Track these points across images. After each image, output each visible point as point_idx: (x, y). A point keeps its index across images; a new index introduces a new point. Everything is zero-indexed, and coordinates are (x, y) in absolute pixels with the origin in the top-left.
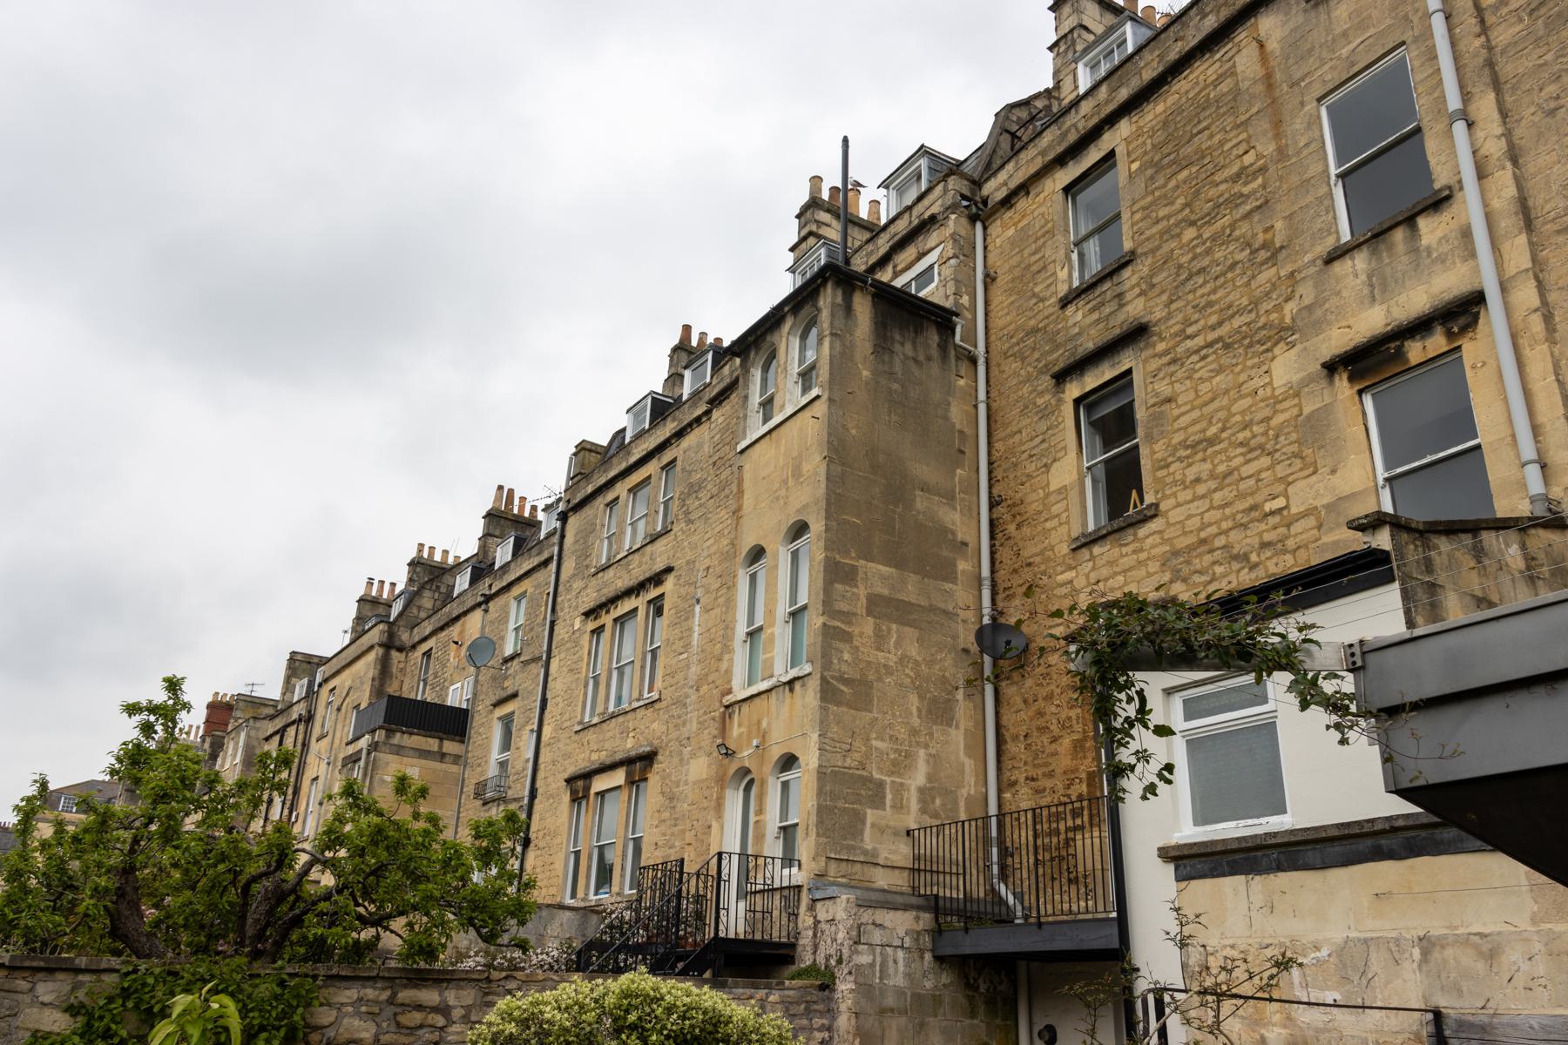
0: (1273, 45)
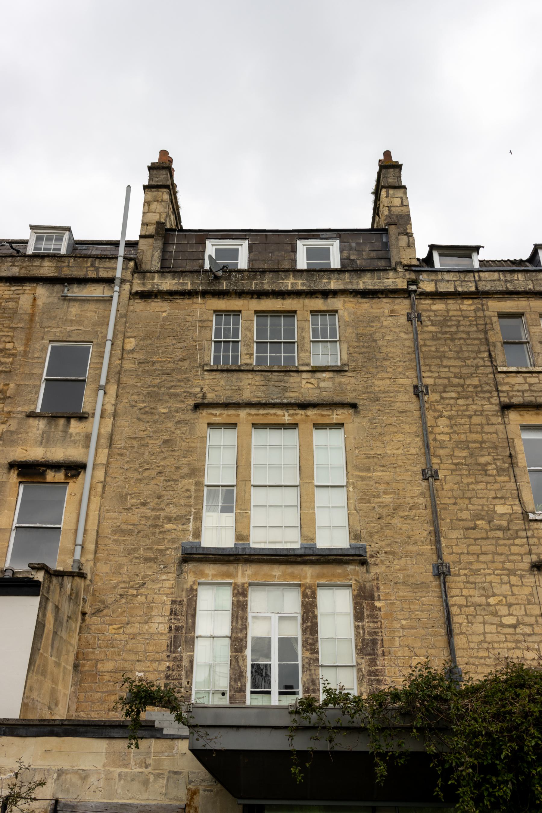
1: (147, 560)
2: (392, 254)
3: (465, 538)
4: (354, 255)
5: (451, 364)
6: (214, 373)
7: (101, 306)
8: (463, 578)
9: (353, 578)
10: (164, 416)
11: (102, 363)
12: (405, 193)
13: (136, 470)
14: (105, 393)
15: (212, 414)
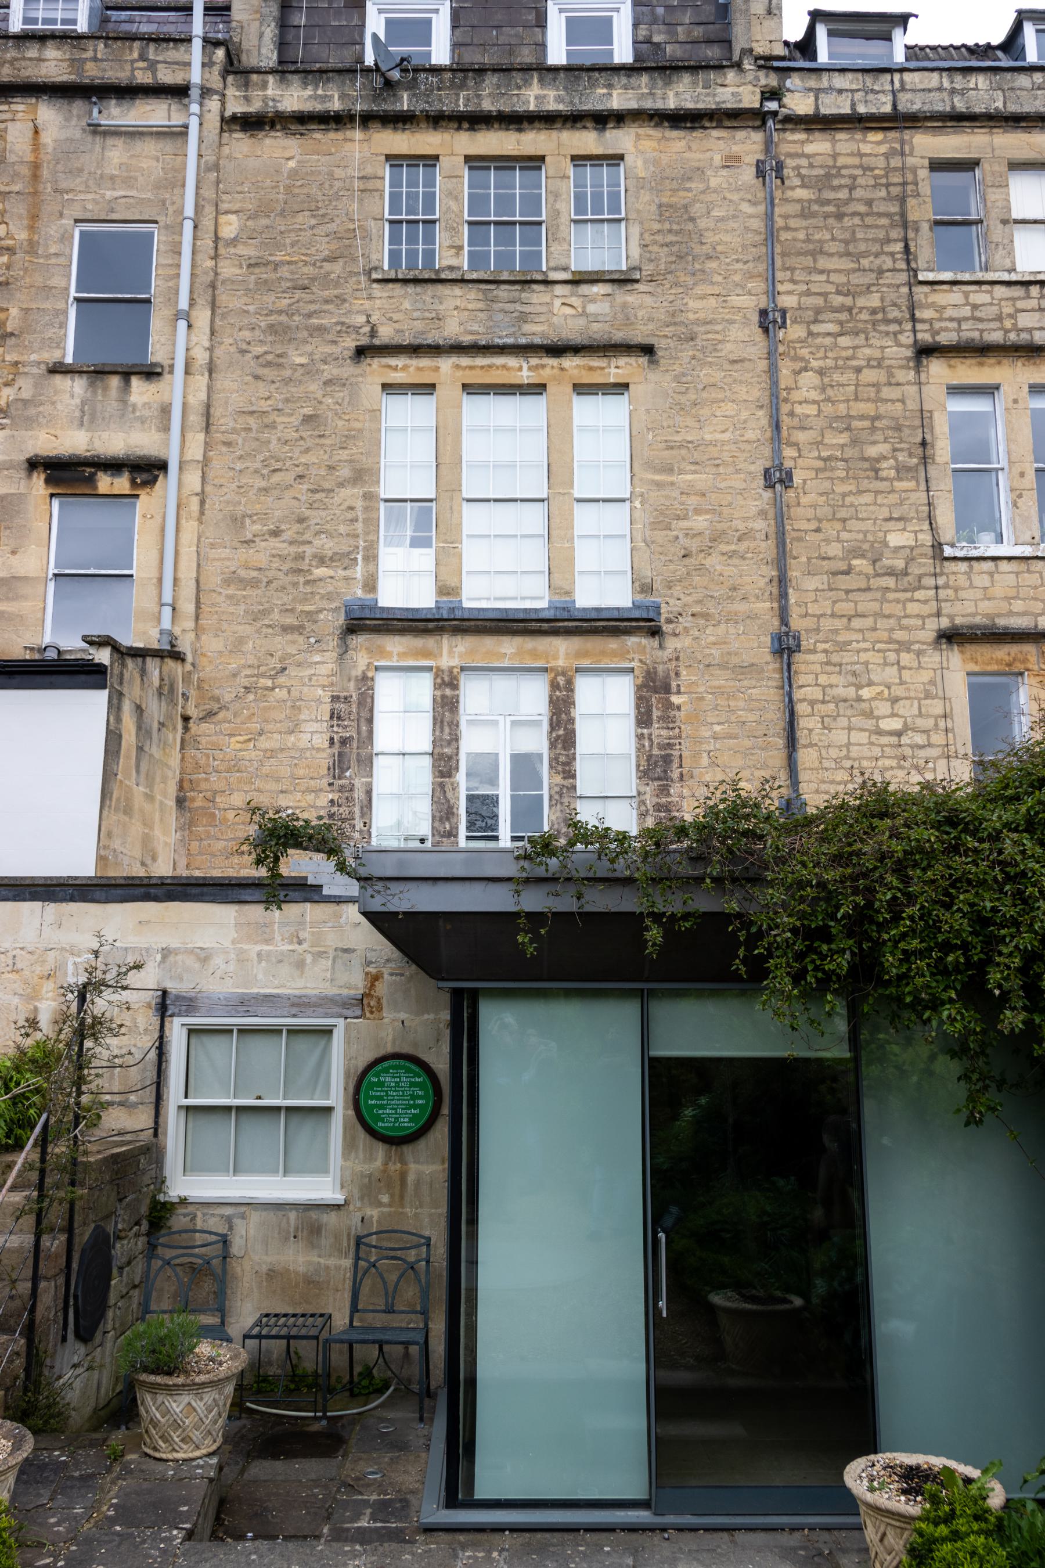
0: (47, 138)
1: (286, 629)
3: (831, 590)
4: (660, 32)
6: (390, 285)
8: (822, 657)
9: (637, 657)
13: (256, 471)
14: (190, 326)
15: (390, 367)
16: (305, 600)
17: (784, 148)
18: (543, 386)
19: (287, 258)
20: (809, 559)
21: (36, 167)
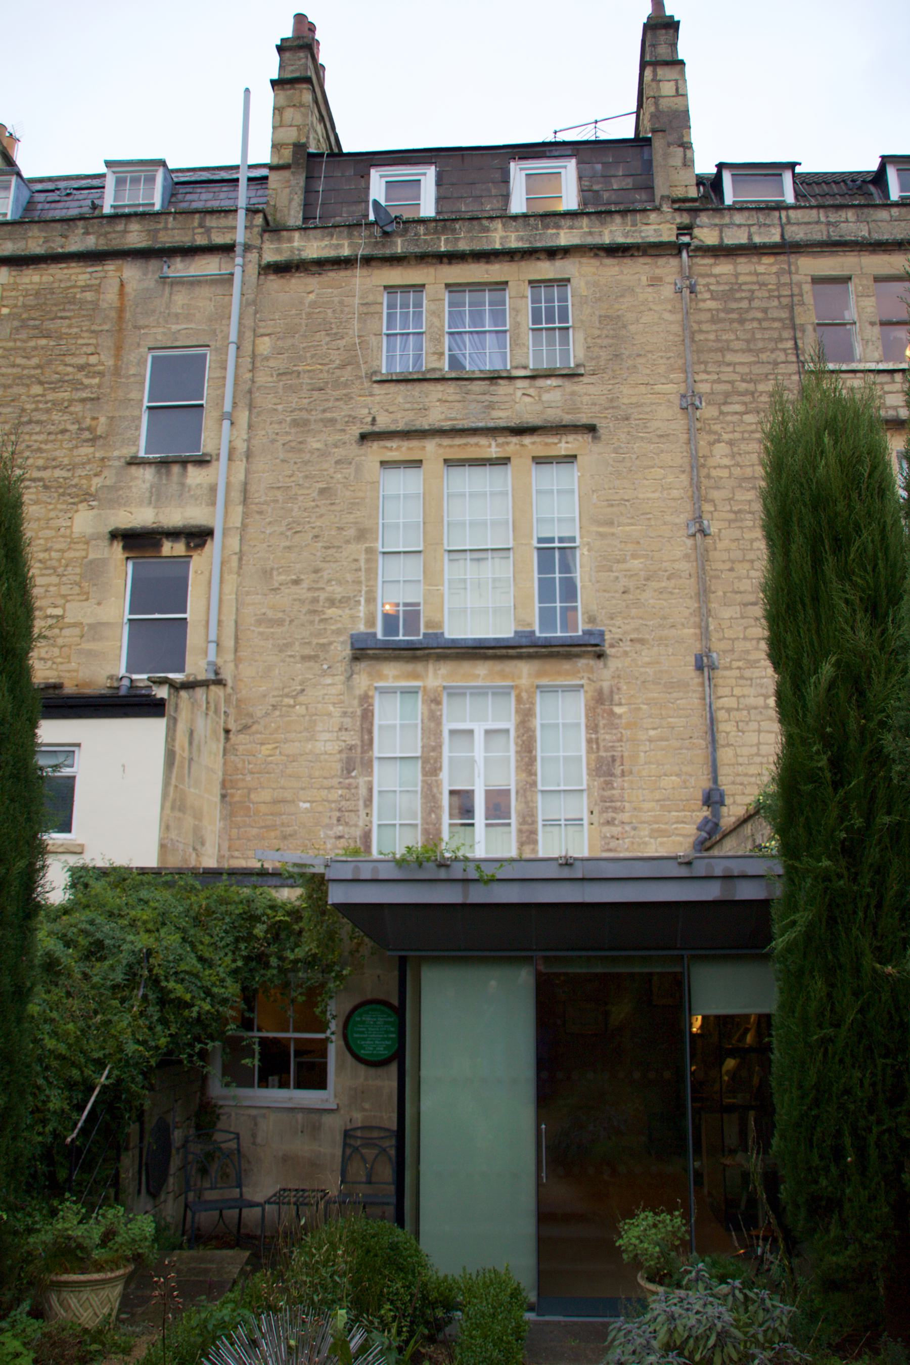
1: (305, 658)
2: (656, 181)
3: (743, 617)
4: (598, 183)
5: (737, 361)
6: (387, 385)
7: (219, 290)
8: (736, 673)
9: (586, 675)
10: (317, 454)
11: (224, 378)
12: (682, 73)
13: (282, 534)
14: (232, 424)
15: (386, 448)
16: (319, 634)
17: (696, 270)
18: (509, 459)
19: (309, 368)
20: (724, 593)
21: (121, 310)
